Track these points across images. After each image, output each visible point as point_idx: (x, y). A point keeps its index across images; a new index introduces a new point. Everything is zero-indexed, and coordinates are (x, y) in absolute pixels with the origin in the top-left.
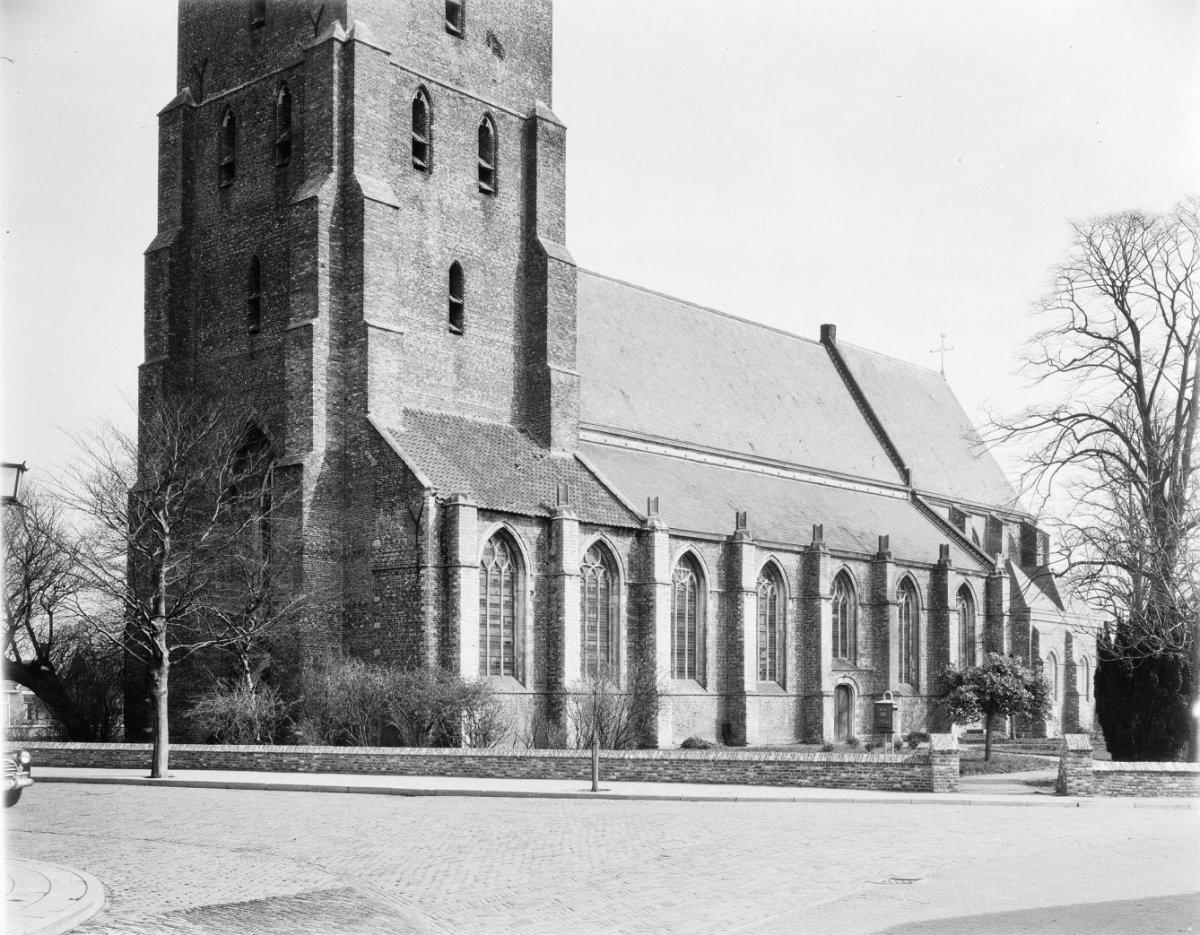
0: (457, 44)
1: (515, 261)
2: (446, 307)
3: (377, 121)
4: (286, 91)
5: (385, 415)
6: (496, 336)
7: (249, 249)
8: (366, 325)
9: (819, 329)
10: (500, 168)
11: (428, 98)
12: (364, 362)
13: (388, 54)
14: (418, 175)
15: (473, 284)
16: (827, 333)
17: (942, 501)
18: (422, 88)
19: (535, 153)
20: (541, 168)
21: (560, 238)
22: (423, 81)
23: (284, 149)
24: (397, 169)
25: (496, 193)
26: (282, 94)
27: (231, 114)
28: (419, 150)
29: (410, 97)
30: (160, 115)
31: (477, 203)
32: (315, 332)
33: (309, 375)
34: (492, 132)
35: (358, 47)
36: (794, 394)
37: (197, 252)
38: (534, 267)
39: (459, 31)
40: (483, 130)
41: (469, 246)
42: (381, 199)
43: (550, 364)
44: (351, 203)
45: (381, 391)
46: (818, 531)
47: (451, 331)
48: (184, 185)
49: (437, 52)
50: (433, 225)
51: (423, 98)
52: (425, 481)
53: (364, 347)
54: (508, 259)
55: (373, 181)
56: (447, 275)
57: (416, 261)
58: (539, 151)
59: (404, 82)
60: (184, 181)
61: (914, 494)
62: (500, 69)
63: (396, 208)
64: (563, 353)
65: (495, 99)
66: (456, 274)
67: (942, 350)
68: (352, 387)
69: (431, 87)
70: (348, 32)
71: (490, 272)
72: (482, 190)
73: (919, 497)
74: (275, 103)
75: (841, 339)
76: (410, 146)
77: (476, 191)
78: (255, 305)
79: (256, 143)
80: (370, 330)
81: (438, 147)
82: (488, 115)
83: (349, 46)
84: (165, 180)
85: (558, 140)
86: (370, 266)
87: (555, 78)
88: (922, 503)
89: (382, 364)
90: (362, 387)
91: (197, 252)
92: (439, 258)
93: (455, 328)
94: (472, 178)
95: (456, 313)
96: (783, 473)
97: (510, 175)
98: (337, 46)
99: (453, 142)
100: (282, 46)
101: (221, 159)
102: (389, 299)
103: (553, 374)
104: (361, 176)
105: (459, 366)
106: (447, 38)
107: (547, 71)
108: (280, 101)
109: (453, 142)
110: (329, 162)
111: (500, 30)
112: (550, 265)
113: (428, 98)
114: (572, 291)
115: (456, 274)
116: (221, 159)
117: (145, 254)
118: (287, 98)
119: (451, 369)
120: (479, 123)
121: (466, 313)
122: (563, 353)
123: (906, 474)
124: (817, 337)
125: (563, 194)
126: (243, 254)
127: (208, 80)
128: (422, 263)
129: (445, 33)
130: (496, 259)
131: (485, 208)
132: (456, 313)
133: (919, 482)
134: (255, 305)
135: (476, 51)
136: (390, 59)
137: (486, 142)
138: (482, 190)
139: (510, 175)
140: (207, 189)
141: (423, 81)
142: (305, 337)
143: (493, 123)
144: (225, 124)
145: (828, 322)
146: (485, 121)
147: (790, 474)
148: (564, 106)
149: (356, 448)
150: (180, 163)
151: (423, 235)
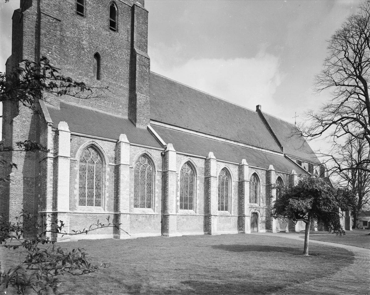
75: (263, 110)
77: (107, 28)
92: (89, 49)
115: (97, 56)
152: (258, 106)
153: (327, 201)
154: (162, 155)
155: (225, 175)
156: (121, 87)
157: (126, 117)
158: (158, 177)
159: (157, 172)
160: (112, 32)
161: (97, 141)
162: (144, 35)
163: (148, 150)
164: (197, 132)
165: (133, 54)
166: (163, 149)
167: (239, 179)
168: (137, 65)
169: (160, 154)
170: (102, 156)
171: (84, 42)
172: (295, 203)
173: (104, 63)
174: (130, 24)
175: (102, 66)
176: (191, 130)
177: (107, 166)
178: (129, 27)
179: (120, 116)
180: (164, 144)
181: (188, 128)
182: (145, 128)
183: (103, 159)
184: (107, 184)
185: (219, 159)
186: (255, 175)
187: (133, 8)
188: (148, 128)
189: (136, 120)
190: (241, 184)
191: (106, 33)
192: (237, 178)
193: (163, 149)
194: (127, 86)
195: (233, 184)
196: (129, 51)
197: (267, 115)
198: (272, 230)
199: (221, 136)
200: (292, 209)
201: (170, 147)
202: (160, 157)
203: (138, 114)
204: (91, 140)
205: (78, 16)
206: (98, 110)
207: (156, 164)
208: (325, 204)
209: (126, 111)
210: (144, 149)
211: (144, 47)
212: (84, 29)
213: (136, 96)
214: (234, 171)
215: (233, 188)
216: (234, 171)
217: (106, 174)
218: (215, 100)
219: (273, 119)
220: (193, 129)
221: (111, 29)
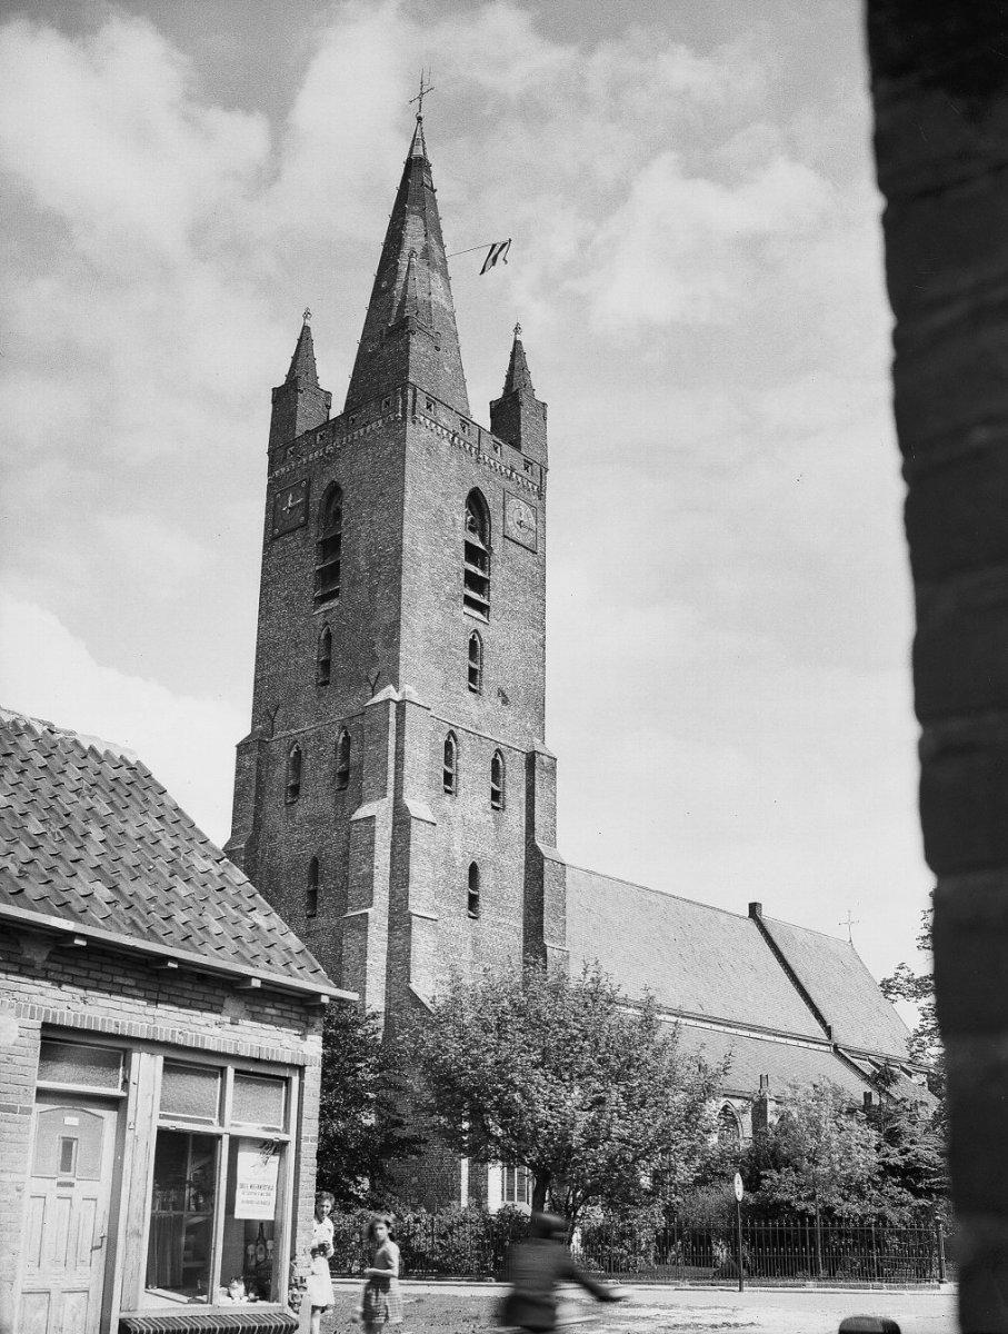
0: (476, 699)
1: (522, 861)
2: (466, 898)
3: (421, 754)
4: (346, 733)
6: (503, 920)
7: (310, 850)
8: (411, 914)
9: (747, 907)
10: (507, 790)
11: (456, 740)
12: (408, 943)
13: (429, 709)
14: (448, 797)
15: (486, 879)
16: (754, 909)
17: (864, 1055)
18: (451, 732)
20: (537, 789)
21: (553, 843)
22: (453, 728)
23: (344, 776)
24: (433, 794)
26: (343, 735)
27: (298, 748)
28: (448, 778)
29: (442, 739)
30: (238, 746)
31: (490, 817)
32: (370, 920)
33: (363, 952)
34: (501, 764)
35: (408, 706)
36: (732, 962)
37: (264, 851)
38: (535, 864)
40: (495, 762)
41: (484, 850)
42: (423, 818)
43: (547, 942)
44: (402, 820)
45: (420, 966)
46: (763, 1079)
47: (470, 917)
48: (257, 801)
49: (461, 706)
50: (457, 836)
51: (452, 740)
53: (408, 931)
54: (515, 862)
55: (417, 805)
56: (467, 872)
57: (445, 863)
58: (536, 776)
59: (439, 729)
60: (256, 796)
61: (836, 1047)
62: (509, 715)
63: (434, 824)
64: (556, 933)
65: (503, 738)
67: (850, 923)
68: (399, 961)
69: (459, 733)
70: (400, 693)
71: (499, 869)
72: (494, 807)
73: (840, 1050)
74: (336, 744)
75: (766, 913)
76: (442, 776)
77: (489, 809)
78: (313, 894)
79: (318, 776)
80: (414, 918)
81: (462, 776)
82: (498, 750)
83: (401, 706)
84: (239, 795)
85: (552, 770)
86: (414, 869)
87: (547, 721)
88: (843, 1056)
89: (423, 944)
90: (407, 964)
91: (264, 851)
92: (462, 859)
93: (472, 914)
95: (473, 901)
96: (728, 1029)
97: (515, 796)
98: (393, 707)
99: (473, 771)
100: (343, 700)
101: (287, 781)
102: (427, 893)
103: (549, 950)
105: (475, 944)
106: (469, 695)
107: (542, 716)
108: (340, 742)
109: (473, 771)
110: (384, 789)
111: (508, 687)
112: (546, 864)
113: (456, 740)
114: (563, 884)
115: (473, 870)
116: (287, 781)
118: (347, 739)
119: (469, 946)
120: (493, 756)
121: (481, 902)
122: (556, 933)
123: (828, 1030)
124: (746, 913)
125: (554, 809)
126: (304, 855)
127: (279, 720)
128: (449, 864)
130: (504, 860)
131: (496, 821)
132: (473, 901)
133: (842, 1036)
134: (313, 894)
135: (491, 703)
136: (431, 713)
137: (496, 771)
138: (494, 807)
139: (515, 796)
140: (275, 805)
141: (453, 728)
142: (362, 924)
143: (502, 756)
144: (292, 755)
145: (753, 901)
147: (733, 1031)
148: (555, 741)
149: (399, 1011)
150: (254, 783)
151: (450, 842)
162: (552, 811)
178: (523, 795)
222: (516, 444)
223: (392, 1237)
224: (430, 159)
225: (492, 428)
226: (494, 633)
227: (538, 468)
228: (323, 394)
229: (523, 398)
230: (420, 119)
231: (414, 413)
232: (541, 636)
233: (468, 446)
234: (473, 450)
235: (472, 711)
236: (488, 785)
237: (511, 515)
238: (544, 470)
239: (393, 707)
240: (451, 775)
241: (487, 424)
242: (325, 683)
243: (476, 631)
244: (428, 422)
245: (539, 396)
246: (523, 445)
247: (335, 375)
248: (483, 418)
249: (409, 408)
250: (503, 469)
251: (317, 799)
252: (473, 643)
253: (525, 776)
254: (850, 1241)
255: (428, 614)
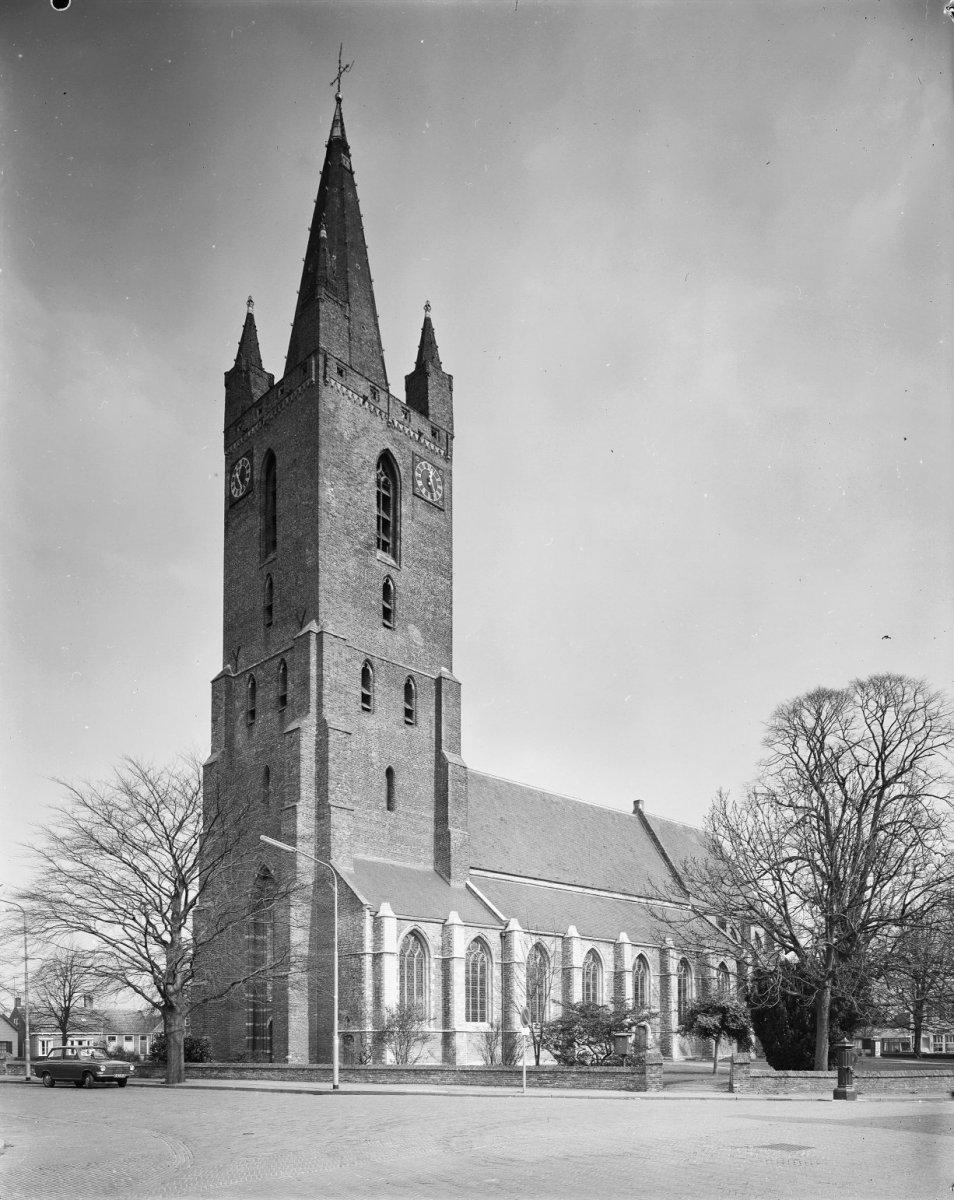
5: (342, 864)
8: (329, 806)
19: (440, 700)
25: (416, 724)
29: (360, 667)
30: (406, 377)
34: (413, 687)
35: (325, 636)
39: (391, 625)
41: (397, 757)
43: (451, 828)
44: (323, 727)
50: (374, 745)
52: (364, 901)
66: (390, 772)
69: (376, 662)
75: (647, 810)
77: (403, 723)
79: (268, 694)
80: (333, 809)
82: (367, 660)
83: (320, 635)
92: (379, 764)
94: (401, 715)
98: (313, 637)
99: (387, 697)
104: (328, 715)
109: (387, 697)
115: (390, 772)
117: (406, 377)
129: (385, 770)
138: (407, 723)
141: (369, 657)
146: (409, 680)
151: (368, 750)
152: (636, 803)
153: (735, 1018)
154: (501, 936)
155: (591, 960)
156: (422, 818)
157: (431, 867)
158: (497, 972)
159: (494, 965)
160: (408, 727)
161: (419, 924)
162: (456, 726)
163: (483, 931)
164: (535, 879)
165: (441, 764)
166: (503, 927)
167: (616, 967)
168: (449, 782)
169: (498, 934)
170: (424, 945)
171: (374, 754)
172: (703, 1020)
173: (399, 782)
174: (433, 707)
175: (397, 789)
176: (526, 877)
177: (432, 960)
178: (432, 714)
179: (420, 867)
180: (504, 918)
181: (522, 874)
182: (463, 886)
183: (426, 950)
184: (433, 987)
185: (585, 937)
186: (641, 957)
187: (439, 681)
188: (468, 887)
189: (449, 875)
190: (618, 976)
191: (402, 732)
192: (613, 966)
193: (503, 927)
194: (430, 814)
195: (606, 976)
196: (433, 754)
197: (655, 819)
198: (671, 1056)
199: (576, 883)
200: (700, 1027)
201: (514, 925)
202: (499, 939)
203: (452, 865)
204: (413, 923)
205: (366, 714)
206: (392, 862)
207: (493, 952)
208: (733, 1021)
209: (430, 857)
210: (477, 930)
211: (456, 748)
212: (373, 732)
213: (449, 833)
214: (606, 953)
215: (605, 983)
216: (606, 953)
217: (432, 971)
218: (557, 803)
219: (669, 827)
220: (529, 875)
221: (407, 723)
222: (424, 412)
223: (859, 916)
224: (350, 141)
225: (407, 401)
226: (405, 580)
227: (443, 436)
228: (266, 376)
229: (430, 368)
230: (339, 100)
231: (325, 377)
232: (449, 582)
233: (378, 411)
234: (384, 414)
235: (382, 642)
236: (402, 704)
237: (415, 472)
238: (450, 437)
239: (313, 637)
240: (369, 696)
241: (402, 396)
242: (270, 625)
243: (389, 576)
244: (339, 386)
245: (446, 368)
246: (431, 412)
247: (274, 361)
248: (399, 390)
249: (321, 372)
250: (412, 433)
251: (267, 718)
252: (386, 587)
253: (428, 698)
254: (933, 926)
255: (342, 565)
